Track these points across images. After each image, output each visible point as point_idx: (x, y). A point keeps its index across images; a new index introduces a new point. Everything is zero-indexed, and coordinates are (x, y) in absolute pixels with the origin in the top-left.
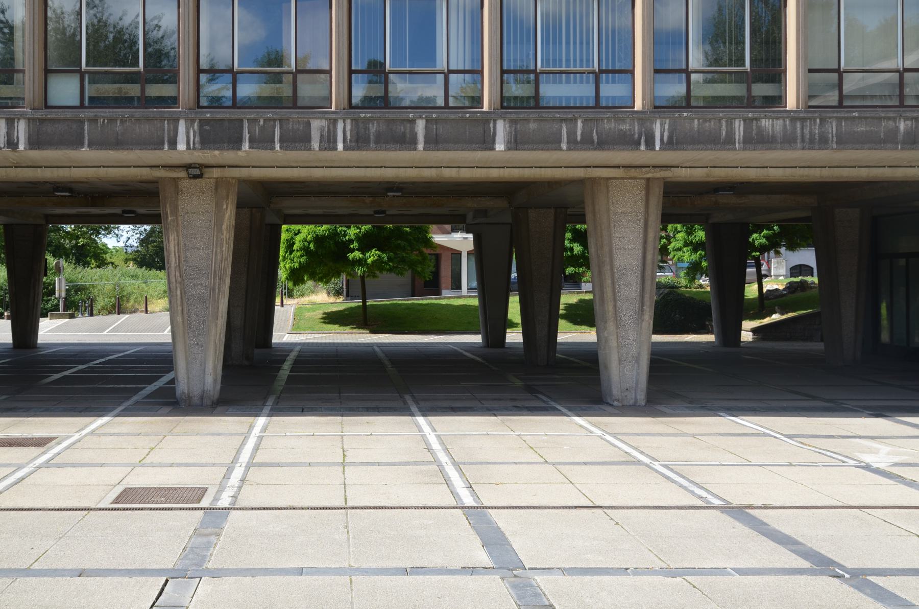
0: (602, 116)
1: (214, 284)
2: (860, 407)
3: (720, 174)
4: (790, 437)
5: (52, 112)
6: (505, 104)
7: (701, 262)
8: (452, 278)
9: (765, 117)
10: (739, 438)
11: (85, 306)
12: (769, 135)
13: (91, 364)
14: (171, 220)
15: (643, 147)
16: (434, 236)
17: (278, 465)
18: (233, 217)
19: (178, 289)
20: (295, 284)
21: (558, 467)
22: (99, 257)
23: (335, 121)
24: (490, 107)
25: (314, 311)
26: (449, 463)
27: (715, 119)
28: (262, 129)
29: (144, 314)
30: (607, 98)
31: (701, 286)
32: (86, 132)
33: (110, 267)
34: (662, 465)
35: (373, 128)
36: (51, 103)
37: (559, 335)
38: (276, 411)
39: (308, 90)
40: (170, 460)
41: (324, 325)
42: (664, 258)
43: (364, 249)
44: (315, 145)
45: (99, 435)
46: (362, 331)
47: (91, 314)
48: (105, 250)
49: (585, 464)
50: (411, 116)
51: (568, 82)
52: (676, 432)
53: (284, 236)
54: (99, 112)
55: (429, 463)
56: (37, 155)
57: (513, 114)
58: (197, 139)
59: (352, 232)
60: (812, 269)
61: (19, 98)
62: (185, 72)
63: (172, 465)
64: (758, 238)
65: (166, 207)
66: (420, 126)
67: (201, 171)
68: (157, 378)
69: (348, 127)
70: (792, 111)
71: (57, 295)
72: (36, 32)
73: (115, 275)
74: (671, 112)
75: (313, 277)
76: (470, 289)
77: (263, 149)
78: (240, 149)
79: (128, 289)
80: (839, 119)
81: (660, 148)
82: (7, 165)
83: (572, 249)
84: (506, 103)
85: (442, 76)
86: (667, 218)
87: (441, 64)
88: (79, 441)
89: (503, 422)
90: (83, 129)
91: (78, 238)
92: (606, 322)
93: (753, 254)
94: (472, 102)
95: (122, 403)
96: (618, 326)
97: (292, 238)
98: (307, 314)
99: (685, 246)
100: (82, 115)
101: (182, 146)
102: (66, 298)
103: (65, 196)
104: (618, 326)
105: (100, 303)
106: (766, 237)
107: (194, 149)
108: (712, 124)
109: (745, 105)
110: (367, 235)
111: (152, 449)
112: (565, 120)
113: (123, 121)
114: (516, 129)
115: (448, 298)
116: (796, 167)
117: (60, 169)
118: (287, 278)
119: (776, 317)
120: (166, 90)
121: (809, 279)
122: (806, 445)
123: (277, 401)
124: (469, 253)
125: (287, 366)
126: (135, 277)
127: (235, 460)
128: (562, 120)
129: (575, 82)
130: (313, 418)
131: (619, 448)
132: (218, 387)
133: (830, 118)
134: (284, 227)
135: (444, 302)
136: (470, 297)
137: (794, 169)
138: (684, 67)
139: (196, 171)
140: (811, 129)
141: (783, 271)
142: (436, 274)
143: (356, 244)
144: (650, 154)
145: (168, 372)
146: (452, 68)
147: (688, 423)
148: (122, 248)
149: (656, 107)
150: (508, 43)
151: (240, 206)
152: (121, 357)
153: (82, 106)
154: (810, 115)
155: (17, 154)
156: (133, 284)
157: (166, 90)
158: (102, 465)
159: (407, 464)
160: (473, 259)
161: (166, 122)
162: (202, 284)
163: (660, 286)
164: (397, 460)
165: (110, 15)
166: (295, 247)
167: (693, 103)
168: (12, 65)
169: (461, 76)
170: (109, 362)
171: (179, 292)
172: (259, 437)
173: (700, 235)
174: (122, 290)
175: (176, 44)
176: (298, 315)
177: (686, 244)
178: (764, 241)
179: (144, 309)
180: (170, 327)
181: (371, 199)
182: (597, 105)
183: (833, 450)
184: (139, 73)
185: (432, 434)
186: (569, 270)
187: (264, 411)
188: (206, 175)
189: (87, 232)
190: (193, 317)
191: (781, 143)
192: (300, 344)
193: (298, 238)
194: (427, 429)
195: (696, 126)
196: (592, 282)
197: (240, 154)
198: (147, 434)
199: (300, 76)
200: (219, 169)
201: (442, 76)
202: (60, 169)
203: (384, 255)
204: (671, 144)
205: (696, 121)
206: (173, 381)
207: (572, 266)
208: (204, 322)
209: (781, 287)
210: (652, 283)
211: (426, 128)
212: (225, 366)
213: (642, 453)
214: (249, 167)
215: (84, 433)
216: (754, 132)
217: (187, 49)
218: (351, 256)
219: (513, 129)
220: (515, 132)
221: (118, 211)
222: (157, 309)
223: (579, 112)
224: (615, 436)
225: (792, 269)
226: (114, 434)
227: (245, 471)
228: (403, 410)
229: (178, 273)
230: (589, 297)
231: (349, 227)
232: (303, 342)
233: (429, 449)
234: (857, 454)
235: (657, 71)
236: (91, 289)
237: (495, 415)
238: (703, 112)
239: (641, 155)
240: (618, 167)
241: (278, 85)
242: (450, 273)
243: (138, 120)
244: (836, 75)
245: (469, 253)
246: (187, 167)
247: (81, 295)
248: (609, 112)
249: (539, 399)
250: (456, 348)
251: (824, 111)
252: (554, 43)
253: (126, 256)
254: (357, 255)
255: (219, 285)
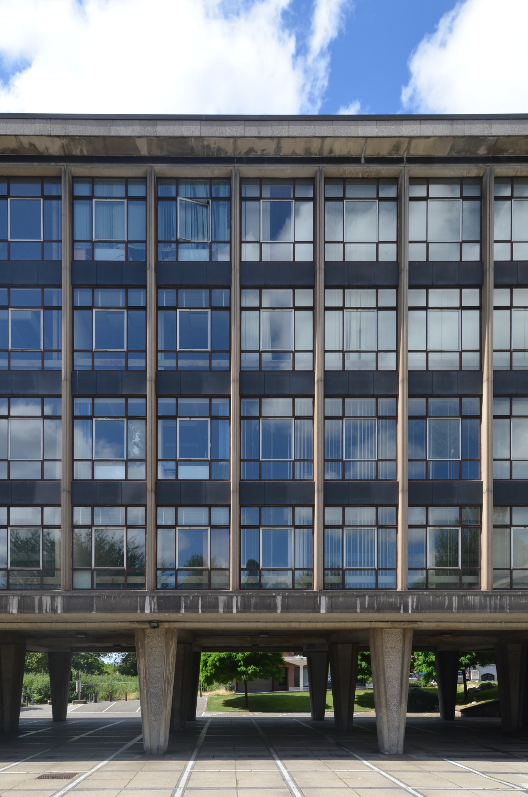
0: (379, 594)
1: (165, 687)
2: (522, 756)
3: (444, 626)
4: (483, 773)
5: (76, 592)
6: (326, 588)
7: (432, 673)
8: (294, 681)
9: (470, 595)
10: (455, 773)
11: (92, 697)
12: (471, 604)
13: (96, 730)
14: (141, 652)
15: (402, 611)
16: (284, 658)
17: (201, 789)
18: (175, 650)
19: (145, 690)
20: (208, 685)
21: (356, 790)
22: (100, 669)
23: (232, 597)
24: (317, 589)
25: (219, 699)
26: (295, 788)
27: (442, 595)
28: (192, 601)
29: (124, 701)
30: (382, 584)
31: (432, 686)
32: (95, 603)
33: (106, 675)
34: (413, 789)
35: (253, 601)
36: (75, 587)
37: (354, 713)
38: (199, 757)
39: (217, 579)
40: (141, 786)
41: (224, 707)
42: (412, 670)
43: (246, 665)
44: (221, 610)
45: (102, 772)
46: (245, 710)
47: (96, 701)
48: (103, 664)
49: (370, 788)
50: (274, 594)
51: (360, 575)
52: (420, 770)
53: (202, 658)
54: (102, 592)
55: (284, 788)
56: (67, 616)
57: (330, 593)
58: (156, 607)
59: (240, 656)
60: (493, 676)
61: (56, 585)
62: (149, 569)
63: (142, 789)
64: (464, 660)
65: (138, 644)
66: (279, 599)
67: (158, 624)
68: (133, 738)
69: (239, 600)
70: (484, 591)
71: (77, 691)
72: (67, 548)
73: (109, 679)
74: (417, 592)
75: (218, 680)
76: (304, 687)
77: (192, 612)
78: (179, 612)
79: (116, 687)
80: (510, 596)
81: (411, 612)
82: (51, 621)
83: (361, 665)
84: (326, 587)
85: (291, 572)
86: (415, 648)
87: (291, 565)
88: (91, 775)
89: (324, 763)
90: (93, 601)
91: (88, 658)
92: (381, 708)
93: (462, 668)
94: (308, 586)
95: (114, 752)
96: (388, 710)
97: (207, 659)
98: (215, 701)
99: (423, 664)
100: (92, 594)
101: (147, 611)
102: (82, 693)
103: (82, 637)
104: (388, 710)
105: (101, 695)
106: (469, 659)
107: (154, 612)
108: (440, 599)
109: (458, 588)
110: (248, 657)
111: (131, 779)
112: (359, 596)
113: (115, 597)
114: (332, 601)
115: (292, 692)
116: (486, 622)
117: (80, 623)
118: (204, 681)
119: (474, 703)
120: (138, 580)
121: (492, 682)
122: (492, 778)
123: (199, 752)
124: (304, 667)
125: (204, 731)
126: (120, 680)
127: (177, 786)
128: (357, 596)
129: (364, 575)
130: (219, 761)
131: (389, 779)
132: (167, 744)
133: (505, 595)
134: (202, 653)
135: (290, 694)
136: (305, 691)
137: (485, 623)
138: (425, 567)
139: (155, 624)
140: (495, 601)
141: (477, 677)
142: (286, 679)
143: (242, 663)
144: (406, 615)
145: (139, 735)
146: (296, 567)
147: (426, 765)
148: (112, 664)
149: (409, 589)
150: (328, 552)
151: (179, 643)
152: (113, 726)
153: (92, 588)
154: (494, 594)
155: (56, 615)
156: (118, 684)
157: (138, 580)
158: (103, 789)
159: (272, 788)
160: (306, 670)
161: (139, 598)
162: (158, 687)
163: (411, 686)
164: (266, 786)
165: (107, 536)
166: (208, 664)
167: (430, 587)
168: (54, 566)
169: (301, 572)
170: (106, 729)
171: (145, 691)
172: (190, 772)
173: (432, 658)
174: (113, 687)
175: (144, 552)
176: (210, 702)
177: (424, 662)
178: (467, 661)
179: (125, 698)
180: (140, 707)
181: (251, 638)
182: (377, 588)
183: (508, 781)
184: (124, 570)
185: (285, 770)
186: (359, 677)
187: (192, 757)
188: (161, 627)
189: (93, 656)
190: (153, 705)
191: (478, 609)
192: (211, 718)
193: (210, 659)
194: (282, 768)
195: (431, 600)
196: (373, 682)
197: (180, 615)
198: (128, 771)
199: (212, 572)
200: (168, 623)
201: (291, 572)
202: (80, 624)
203: (258, 669)
204: (417, 609)
205: (431, 597)
206: (142, 740)
207: (361, 675)
208: (159, 708)
209: (477, 687)
210: (407, 684)
211: (282, 600)
212: (171, 732)
213: (402, 782)
214: (184, 622)
215: (93, 770)
216: (464, 603)
217: (150, 557)
218: (239, 669)
219: (330, 601)
220: (332, 603)
221: (111, 645)
222: (132, 698)
223: (367, 592)
224: (386, 772)
225: (482, 676)
226: (110, 771)
227: (182, 792)
228: (268, 756)
229: (145, 681)
230: (371, 691)
231: (238, 653)
232: (213, 717)
233: (284, 779)
234: (521, 783)
235: (410, 569)
236: (96, 687)
237: (320, 760)
238: (435, 592)
239: (401, 615)
240: (388, 622)
241: (200, 577)
242: (293, 678)
243: (123, 596)
244: (509, 571)
245: (304, 667)
246: (150, 622)
247: (90, 691)
248: (383, 592)
249: (344, 750)
250: (298, 721)
251: (502, 592)
252: (353, 552)
253: (115, 669)
254: (243, 668)
255: (168, 687)
